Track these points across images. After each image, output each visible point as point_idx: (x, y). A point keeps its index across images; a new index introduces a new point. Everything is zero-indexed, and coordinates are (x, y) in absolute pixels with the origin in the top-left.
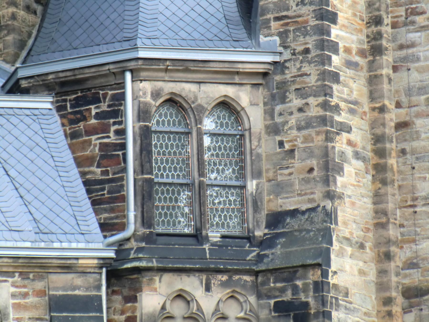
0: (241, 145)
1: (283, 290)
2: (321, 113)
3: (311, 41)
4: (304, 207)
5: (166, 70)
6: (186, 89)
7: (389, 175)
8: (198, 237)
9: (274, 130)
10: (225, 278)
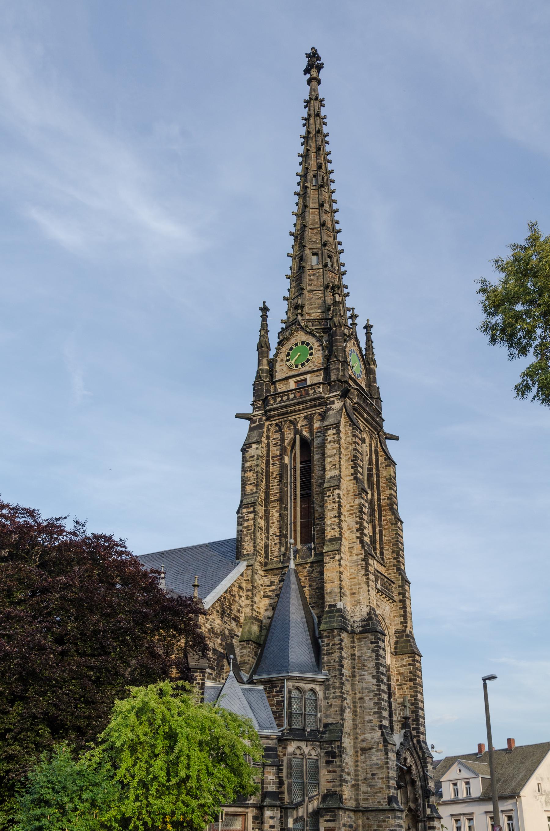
0: (316, 703)
1: (328, 748)
2: (340, 694)
4: (334, 722)
5: (296, 679)
6: (301, 685)
7: (357, 714)
8: (304, 730)
9: (326, 698)
10: (311, 743)
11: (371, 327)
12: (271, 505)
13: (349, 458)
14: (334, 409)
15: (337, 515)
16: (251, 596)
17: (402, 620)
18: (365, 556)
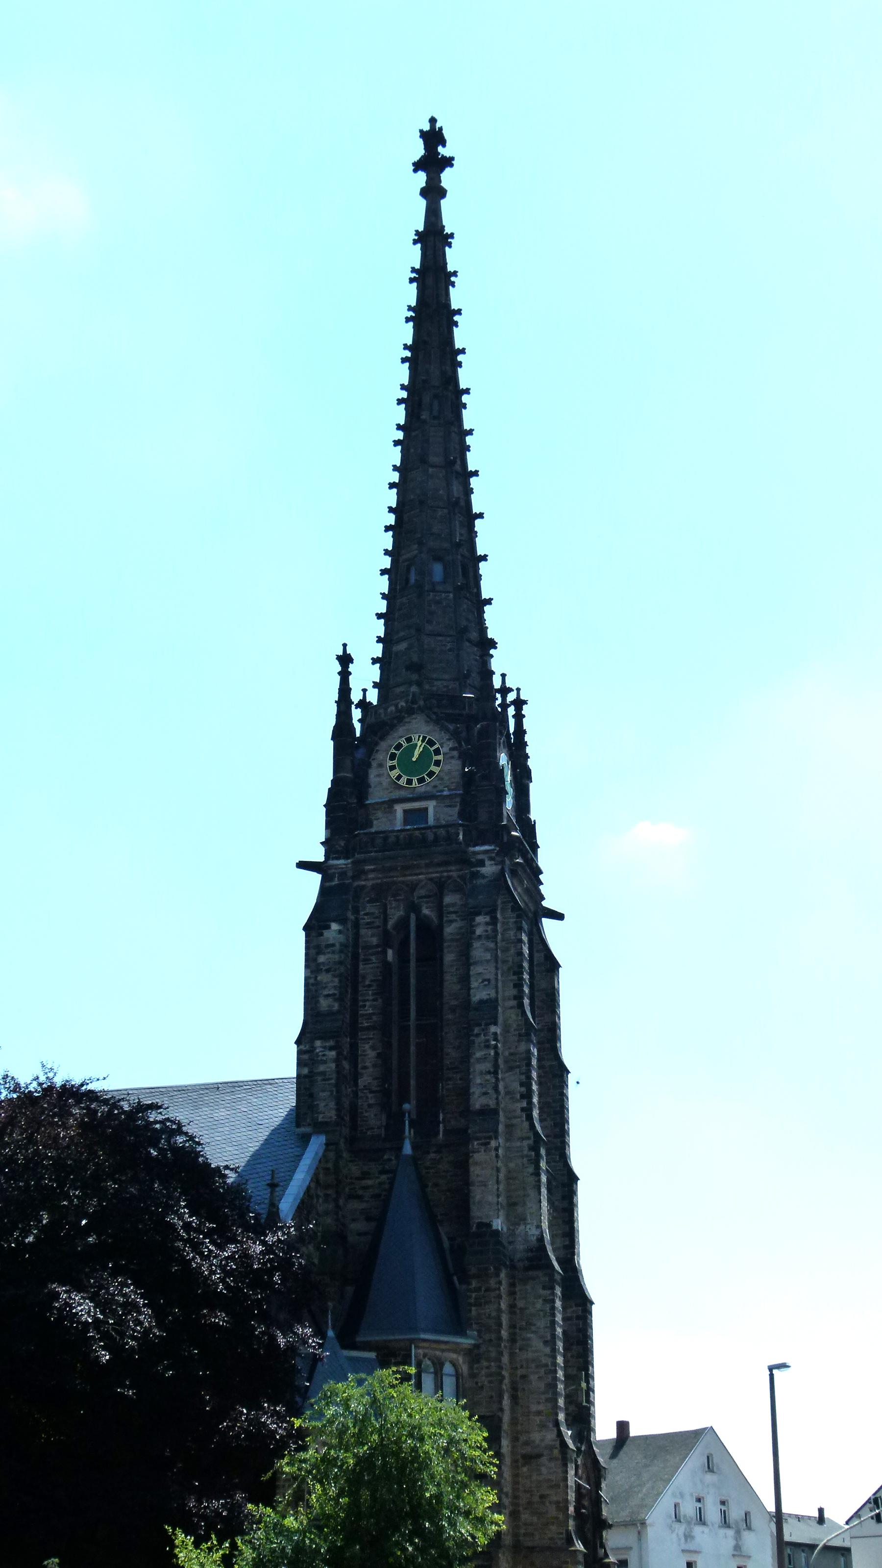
3: (493, 1336)
11: (525, 702)
12: (362, 1035)
13: (509, 969)
14: (483, 877)
15: (492, 1070)
16: (334, 1196)
17: (567, 1243)
18: (535, 1142)
